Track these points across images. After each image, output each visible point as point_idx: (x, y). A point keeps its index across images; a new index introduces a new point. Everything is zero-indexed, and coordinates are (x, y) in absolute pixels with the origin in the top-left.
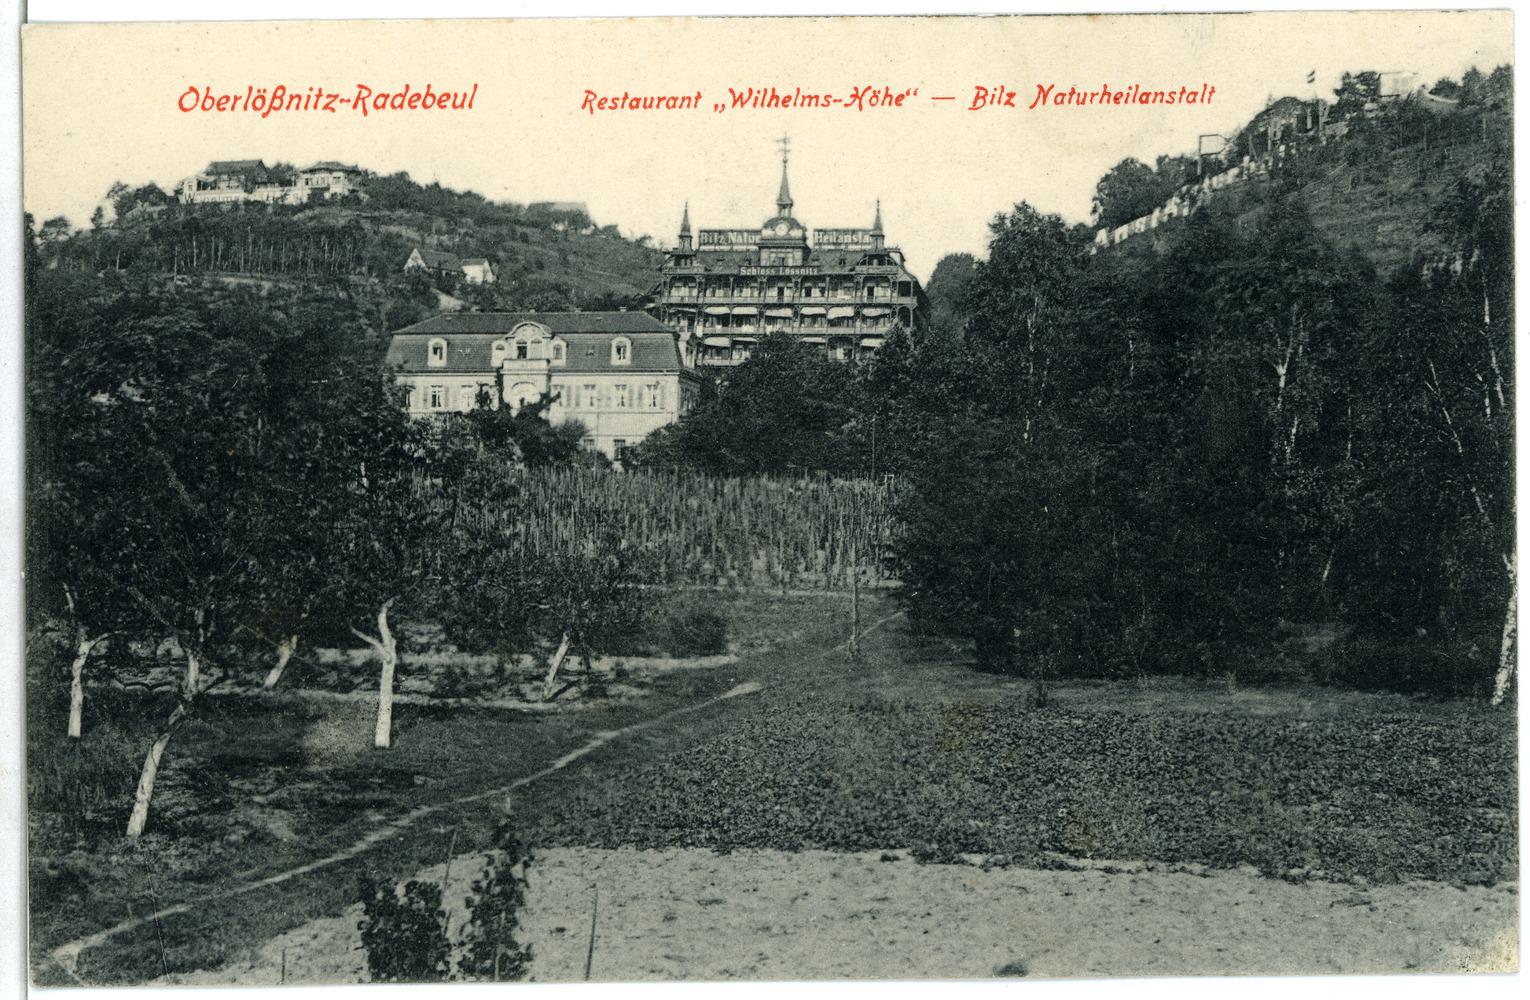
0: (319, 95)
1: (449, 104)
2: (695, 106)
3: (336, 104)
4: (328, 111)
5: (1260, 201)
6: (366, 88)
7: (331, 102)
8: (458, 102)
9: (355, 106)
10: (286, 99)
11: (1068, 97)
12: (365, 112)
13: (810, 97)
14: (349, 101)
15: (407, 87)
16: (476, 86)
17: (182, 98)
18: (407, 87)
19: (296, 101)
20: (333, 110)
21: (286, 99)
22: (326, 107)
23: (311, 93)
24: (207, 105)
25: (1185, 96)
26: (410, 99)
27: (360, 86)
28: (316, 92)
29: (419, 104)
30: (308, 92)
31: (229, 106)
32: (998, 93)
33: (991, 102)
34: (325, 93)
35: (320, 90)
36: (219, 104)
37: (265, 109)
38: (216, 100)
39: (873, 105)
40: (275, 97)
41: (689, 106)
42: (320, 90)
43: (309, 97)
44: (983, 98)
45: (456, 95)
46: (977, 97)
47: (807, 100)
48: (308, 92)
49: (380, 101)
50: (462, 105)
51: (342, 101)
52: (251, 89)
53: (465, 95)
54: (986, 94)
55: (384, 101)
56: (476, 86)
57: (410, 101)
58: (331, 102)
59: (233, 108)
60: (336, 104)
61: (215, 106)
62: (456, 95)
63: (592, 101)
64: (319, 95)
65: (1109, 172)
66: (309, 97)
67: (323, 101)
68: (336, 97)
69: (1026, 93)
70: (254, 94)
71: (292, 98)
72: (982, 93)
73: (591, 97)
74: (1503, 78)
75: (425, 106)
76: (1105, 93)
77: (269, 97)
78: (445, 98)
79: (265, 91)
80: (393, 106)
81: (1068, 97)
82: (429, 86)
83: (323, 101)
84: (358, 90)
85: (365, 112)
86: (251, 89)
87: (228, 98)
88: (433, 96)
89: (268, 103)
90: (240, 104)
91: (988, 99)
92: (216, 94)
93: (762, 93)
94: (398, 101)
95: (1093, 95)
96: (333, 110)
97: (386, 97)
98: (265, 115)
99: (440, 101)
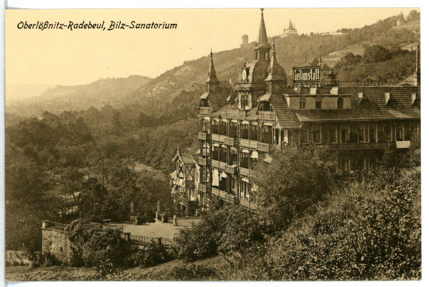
0: (58, 25)
1: (96, 27)
2: (176, 28)
3: (124, 27)
4: (122, 29)
5: (222, 251)
6: (71, 22)
7: (61, 26)
8: (99, 27)
9: (68, 28)
10: (48, 25)
11: (151, 25)
12: (71, 30)
13: (174, 25)
14: (67, 26)
15: (84, 22)
16: (104, 22)
17: (19, 24)
18: (84, 22)
19: (51, 26)
20: (62, 29)
21: (48, 25)
22: (60, 28)
23: (56, 24)
24: (26, 27)
25: (154, 26)
26: (84, 26)
27: (70, 22)
28: (57, 23)
29: (87, 27)
30: (55, 23)
31: (32, 27)
32: (118, 24)
33: (116, 28)
34: (60, 24)
35: (58, 23)
36: (29, 26)
37: (43, 28)
38: (92, 25)
39: (19, 28)
40: (45, 24)
41: (52, 28)
42: (58, 23)
43: (55, 25)
44: (114, 25)
45: (98, 24)
46: (111, 25)
47: (173, 26)
48: (55, 23)
49: (76, 26)
50: (100, 28)
51: (65, 26)
52: (38, 22)
53: (101, 25)
54: (115, 24)
55: (76, 26)
56: (104, 22)
57: (84, 26)
58: (61, 26)
59: (33, 28)
60: (63, 27)
61: (28, 27)
62: (98, 24)
63: (174, 25)
64: (58, 25)
65: (85, 85)
66: (55, 25)
67: (59, 26)
68: (125, 25)
69: (107, 25)
70: (39, 24)
71: (50, 25)
72: (113, 24)
73: (71, 24)
74: (415, 16)
75: (89, 28)
76: (90, 24)
77: (43, 25)
78: (31, 25)
79: (43, 23)
80: (147, 28)
81: (151, 25)
82: (90, 22)
83: (59, 26)
84: (69, 23)
85: (71, 30)
86: (38, 22)
87: (32, 25)
88: (27, 25)
89: (83, 26)
90: (35, 26)
91: (115, 26)
92: (28, 24)
93: (119, 23)
94: (81, 26)
95: (34, 25)
96: (62, 29)
97: (77, 25)
98: (42, 30)
99: (29, 26)
